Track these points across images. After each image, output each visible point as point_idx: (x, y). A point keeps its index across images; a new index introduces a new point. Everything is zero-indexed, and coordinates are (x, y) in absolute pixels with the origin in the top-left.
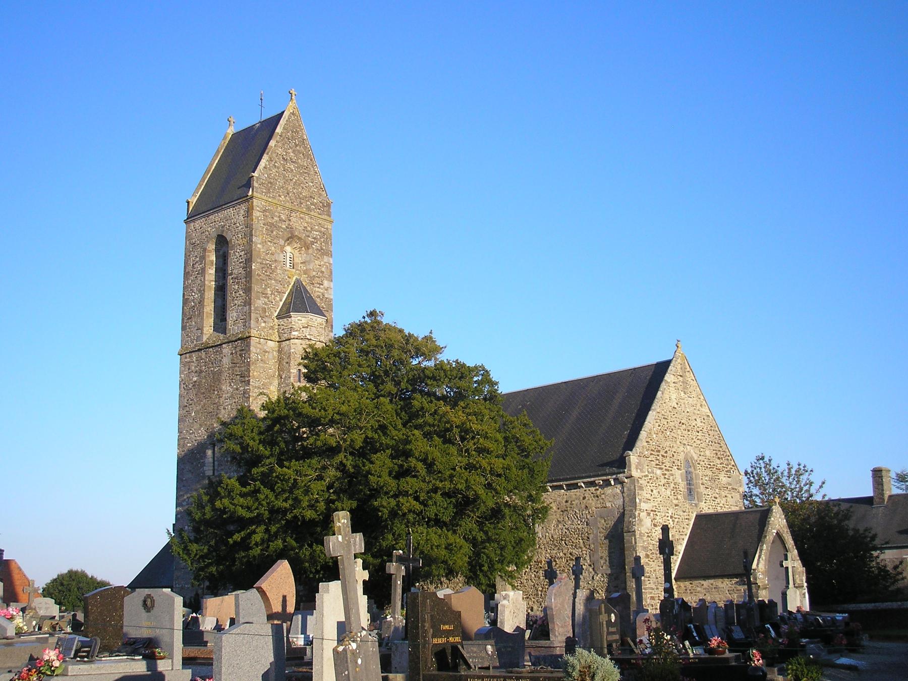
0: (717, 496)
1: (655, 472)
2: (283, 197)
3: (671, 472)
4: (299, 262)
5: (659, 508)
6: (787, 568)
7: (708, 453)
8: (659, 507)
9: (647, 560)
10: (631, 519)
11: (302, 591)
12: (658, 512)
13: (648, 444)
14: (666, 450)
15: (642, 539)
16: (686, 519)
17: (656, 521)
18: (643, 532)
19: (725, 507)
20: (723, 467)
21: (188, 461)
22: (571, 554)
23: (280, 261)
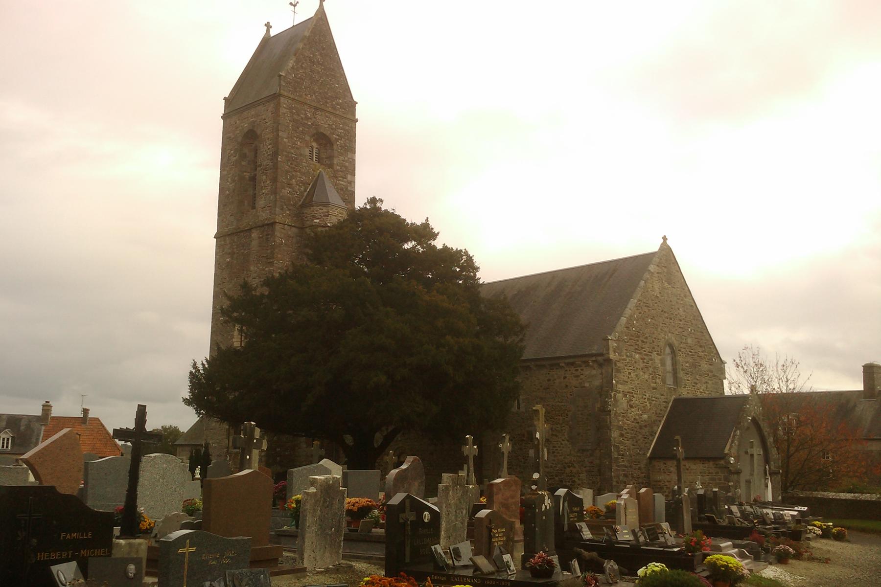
1: (633, 356)
2: (309, 96)
3: (650, 357)
4: (324, 156)
5: (636, 390)
6: (752, 455)
7: (689, 341)
8: (637, 389)
12: (635, 394)
14: (646, 336)
15: (617, 418)
16: (664, 402)
17: (632, 402)
18: (618, 412)
19: (705, 393)
21: (220, 334)
23: (306, 155)
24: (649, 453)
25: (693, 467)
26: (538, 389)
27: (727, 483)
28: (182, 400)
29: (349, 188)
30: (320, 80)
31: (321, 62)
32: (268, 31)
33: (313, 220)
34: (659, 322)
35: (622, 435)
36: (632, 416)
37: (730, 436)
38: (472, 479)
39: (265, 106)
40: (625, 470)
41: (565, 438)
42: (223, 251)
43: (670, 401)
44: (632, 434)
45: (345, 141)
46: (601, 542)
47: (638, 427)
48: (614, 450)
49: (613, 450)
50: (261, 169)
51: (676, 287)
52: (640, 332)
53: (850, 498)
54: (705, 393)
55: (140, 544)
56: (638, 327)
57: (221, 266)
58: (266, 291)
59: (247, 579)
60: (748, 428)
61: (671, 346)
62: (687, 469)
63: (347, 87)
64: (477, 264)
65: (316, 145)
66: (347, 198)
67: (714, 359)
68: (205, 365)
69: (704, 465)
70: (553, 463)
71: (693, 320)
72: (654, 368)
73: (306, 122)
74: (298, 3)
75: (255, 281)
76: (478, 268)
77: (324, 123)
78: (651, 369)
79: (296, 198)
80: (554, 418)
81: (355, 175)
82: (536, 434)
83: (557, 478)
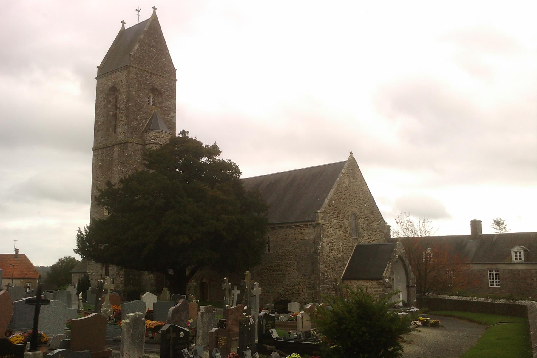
1: (333, 221)
2: (148, 66)
7: (366, 211)
9: (326, 269)
10: (317, 246)
12: (334, 243)
15: (323, 257)
16: (351, 247)
17: (332, 248)
18: (324, 253)
19: (375, 241)
22: (287, 263)
24: (342, 276)
26: (280, 240)
31: (154, 46)
32: (123, 26)
33: (150, 140)
34: (348, 201)
35: (326, 267)
36: (332, 256)
40: (328, 286)
41: (295, 268)
43: (354, 246)
44: (332, 266)
45: (169, 92)
49: (321, 275)
50: (119, 110)
52: (336, 208)
53: (457, 299)
54: (375, 241)
55: (39, 354)
57: (96, 167)
58: (121, 186)
60: (397, 261)
61: (354, 214)
63: (171, 61)
66: (171, 126)
67: (380, 221)
68: (86, 229)
70: (288, 283)
71: (368, 200)
72: (345, 228)
73: (146, 82)
74: (141, 9)
76: (242, 173)
77: (157, 82)
78: (343, 228)
79: (140, 127)
80: (289, 257)
81: (175, 113)
83: (290, 292)
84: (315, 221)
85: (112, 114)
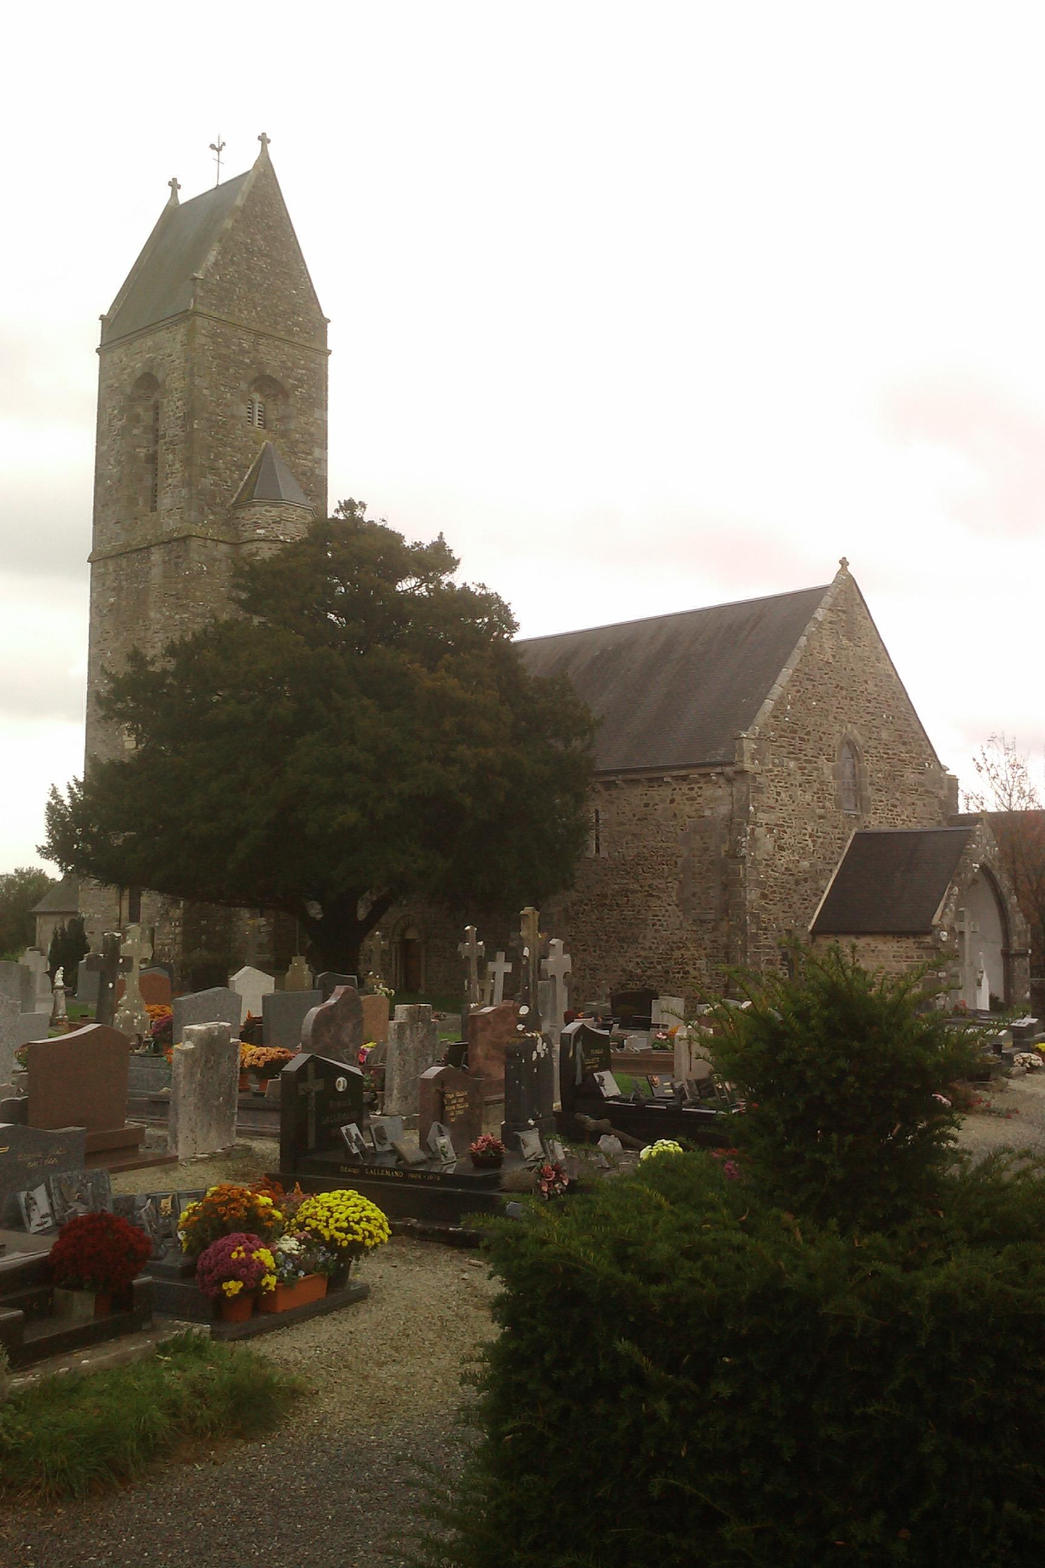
0: (897, 803)
2: (246, 312)
3: (815, 765)
6: (962, 933)
7: (884, 735)
11: (264, 925)
13: (775, 721)
15: (756, 868)
19: (910, 821)
20: (911, 757)
25: (881, 946)
27: (936, 973)
28: (36, 849)
29: (317, 472)
30: (265, 282)
31: (265, 252)
32: (174, 194)
33: (254, 530)
35: (764, 896)
37: (941, 899)
38: (475, 993)
39: (171, 332)
42: (104, 586)
46: (628, 1101)
47: (792, 882)
48: (751, 921)
49: (748, 922)
51: (861, 644)
54: (910, 821)
56: (794, 715)
57: (100, 611)
58: (171, 665)
59: (78, 1185)
60: (975, 881)
62: (873, 951)
64: (516, 619)
65: (259, 396)
66: (314, 489)
67: (926, 764)
68: (73, 789)
69: (899, 945)
70: (653, 943)
72: (822, 783)
73: (241, 358)
75: (157, 637)
77: (272, 358)
78: (816, 785)
79: (225, 492)
81: (327, 449)
82: (523, 950)
83: (659, 967)
84: (732, 764)
85: (146, 455)
